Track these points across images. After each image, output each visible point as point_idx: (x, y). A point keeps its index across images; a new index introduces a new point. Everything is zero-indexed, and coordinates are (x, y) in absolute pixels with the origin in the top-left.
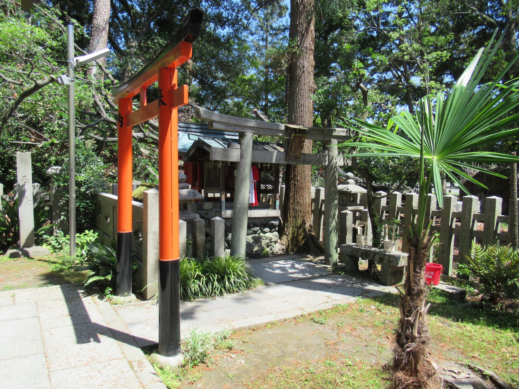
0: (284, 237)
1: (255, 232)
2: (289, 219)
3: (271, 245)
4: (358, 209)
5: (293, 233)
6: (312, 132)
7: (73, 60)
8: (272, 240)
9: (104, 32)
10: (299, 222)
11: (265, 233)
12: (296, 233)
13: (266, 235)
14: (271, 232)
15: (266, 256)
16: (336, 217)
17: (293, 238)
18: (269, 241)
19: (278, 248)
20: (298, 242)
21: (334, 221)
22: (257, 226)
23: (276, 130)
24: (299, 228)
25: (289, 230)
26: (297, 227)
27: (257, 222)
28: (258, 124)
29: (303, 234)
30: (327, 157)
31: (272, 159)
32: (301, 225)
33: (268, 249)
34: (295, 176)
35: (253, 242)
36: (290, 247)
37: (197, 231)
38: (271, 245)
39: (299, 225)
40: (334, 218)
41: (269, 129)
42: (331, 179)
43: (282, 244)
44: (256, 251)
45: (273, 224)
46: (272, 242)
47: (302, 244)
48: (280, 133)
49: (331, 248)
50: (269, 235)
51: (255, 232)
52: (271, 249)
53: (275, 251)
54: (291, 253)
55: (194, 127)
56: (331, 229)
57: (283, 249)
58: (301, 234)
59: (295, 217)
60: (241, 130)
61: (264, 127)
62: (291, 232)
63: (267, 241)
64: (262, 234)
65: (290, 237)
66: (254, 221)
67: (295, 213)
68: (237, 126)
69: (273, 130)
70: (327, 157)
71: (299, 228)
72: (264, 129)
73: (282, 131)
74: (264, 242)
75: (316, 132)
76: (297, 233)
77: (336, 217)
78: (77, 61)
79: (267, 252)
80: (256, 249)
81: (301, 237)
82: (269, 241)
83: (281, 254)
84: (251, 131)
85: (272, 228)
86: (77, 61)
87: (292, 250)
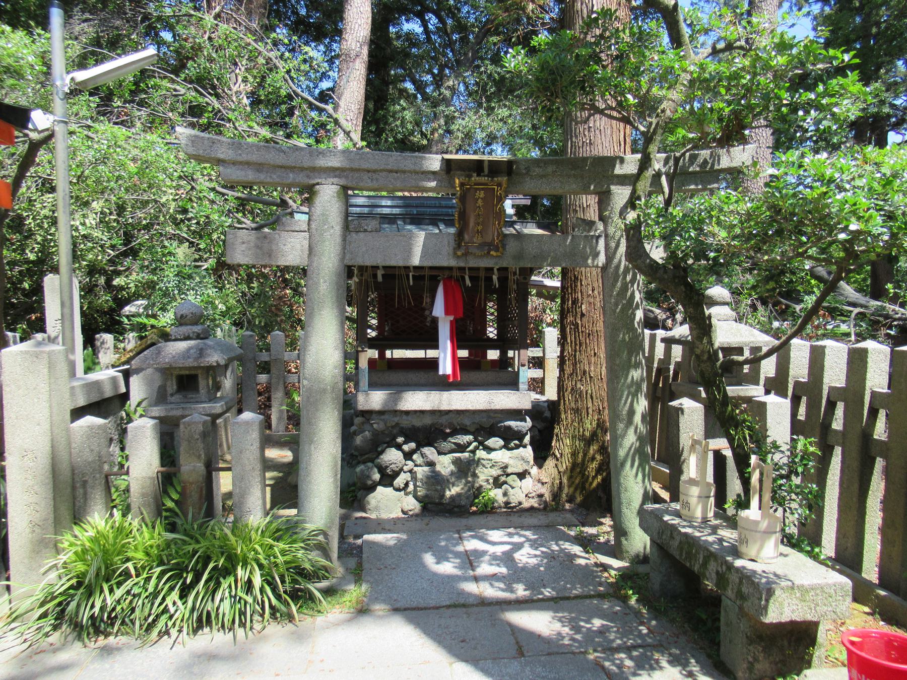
0: (550, 463)
1: (461, 448)
2: (563, 416)
3: (505, 483)
4: (742, 394)
5: (574, 454)
6: (537, 171)
7: (63, 79)
8: (509, 470)
9: (358, 61)
10: (589, 425)
11: (489, 450)
12: (581, 455)
13: (494, 455)
14: (506, 447)
15: (489, 509)
16: (638, 418)
17: (574, 465)
18: (500, 472)
19: (525, 491)
20: (585, 478)
21: (631, 431)
22: (466, 432)
23: (416, 173)
24: (589, 442)
25: (563, 446)
26: (582, 438)
27: (467, 422)
28: (351, 160)
29: (598, 457)
30: (602, 242)
31: (409, 252)
32: (594, 434)
33: (496, 494)
34: (575, 302)
35: (452, 473)
36: (566, 490)
37: (182, 449)
38: (505, 483)
39: (587, 434)
40: (630, 421)
41: (391, 171)
42: (616, 305)
43: (539, 481)
44: (452, 497)
45: (509, 428)
46: (508, 475)
47: (595, 484)
48: (429, 180)
49: (625, 510)
50: (502, 456)
51: (461, 448)
52: (505, 494)
53: (514, 501)
54: (567, 506)
55: (389, 203)
56: (622, 453)
57: (541, 496)
58: (593, 459)
59: (577, 411)
60: (302, 179)
61: (375, 167)
62: (567, 451)
63: (495, 472)
64: (481, 454)
65: (565, 464)
66: (456, 421)
67: (576, 401)
68: (292, 168)
69: (404, 172)
70: (602, 242)
71: (589, 442)
72: (375, 171)
73: (434, 173)
74: (484, 475)
75: (550, 169)
76: (585, 455)
77: (638, 418)
78: (72, 79)
79: (493, 501)
80: (453, 491)
81: (594, 465)
82: (500, 472)
83: (532, 509)
84: (335, 180)
85: (511, 438)
86: (72, 79)
87: (571, 500)
